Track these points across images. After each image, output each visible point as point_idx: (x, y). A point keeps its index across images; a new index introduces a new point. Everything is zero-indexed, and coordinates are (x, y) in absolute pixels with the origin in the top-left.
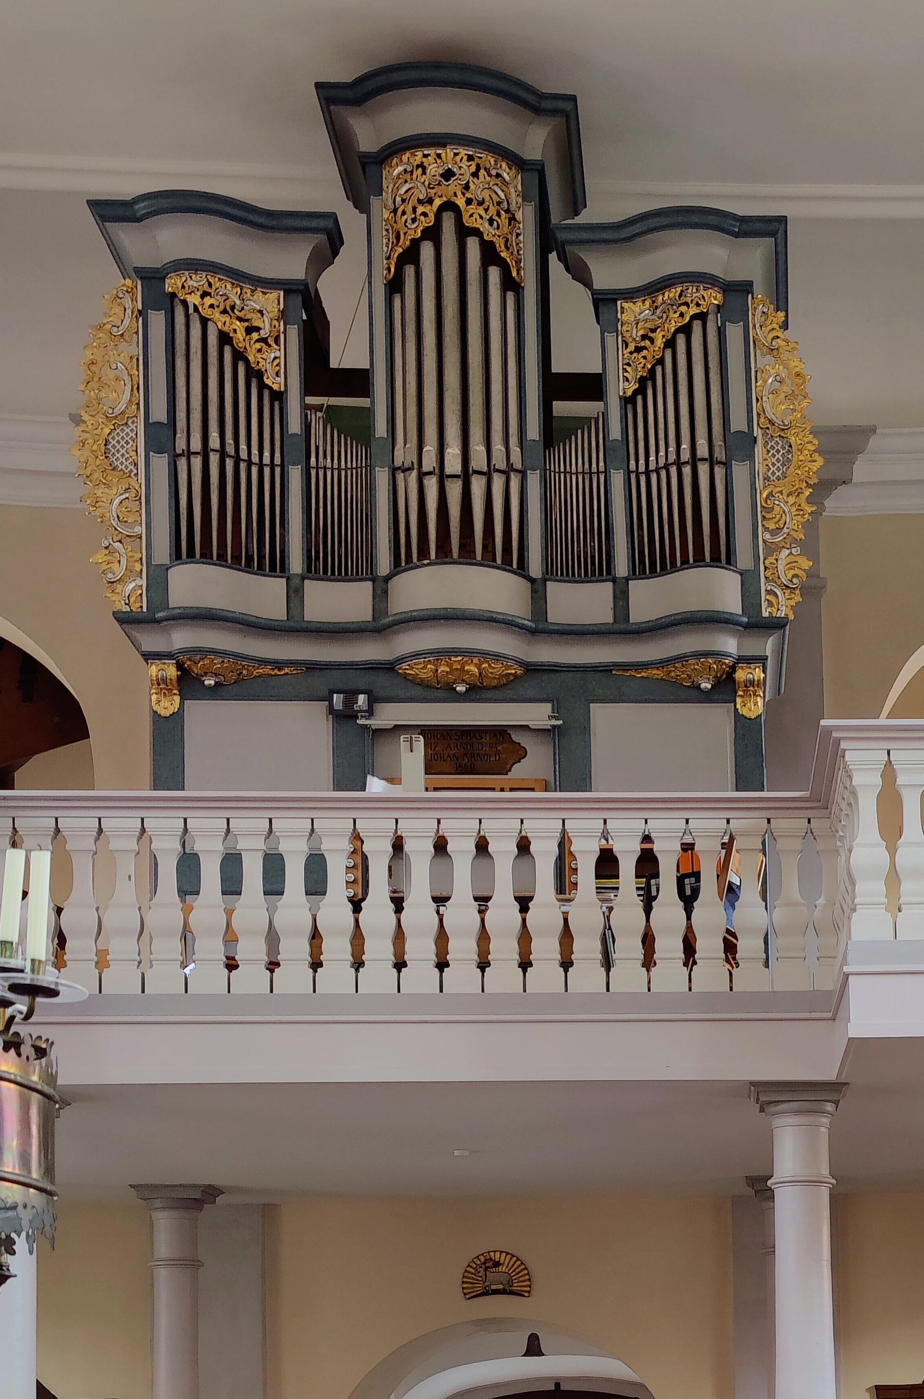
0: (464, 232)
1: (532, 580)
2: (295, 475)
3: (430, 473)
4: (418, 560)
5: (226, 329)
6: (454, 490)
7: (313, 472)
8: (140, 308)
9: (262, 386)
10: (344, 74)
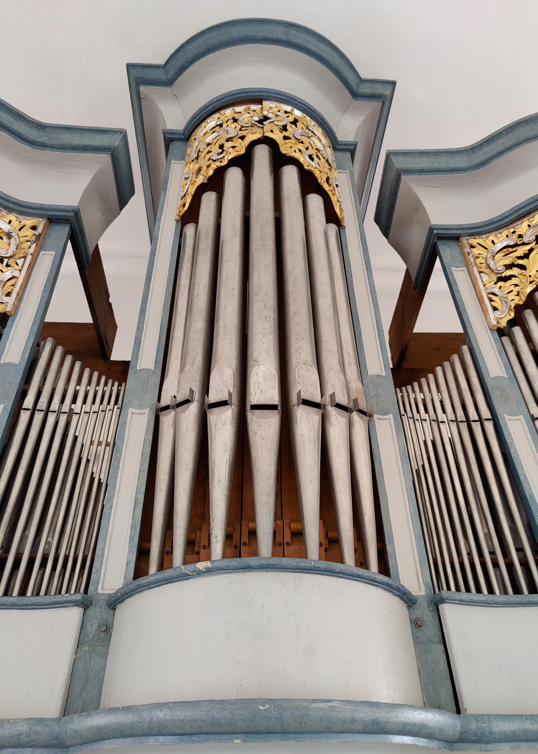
0: (279, 160)
1: (409, 600)
3: (223, 403)
4: (185, 562)
6: (264, 432)
7: (24, 417)
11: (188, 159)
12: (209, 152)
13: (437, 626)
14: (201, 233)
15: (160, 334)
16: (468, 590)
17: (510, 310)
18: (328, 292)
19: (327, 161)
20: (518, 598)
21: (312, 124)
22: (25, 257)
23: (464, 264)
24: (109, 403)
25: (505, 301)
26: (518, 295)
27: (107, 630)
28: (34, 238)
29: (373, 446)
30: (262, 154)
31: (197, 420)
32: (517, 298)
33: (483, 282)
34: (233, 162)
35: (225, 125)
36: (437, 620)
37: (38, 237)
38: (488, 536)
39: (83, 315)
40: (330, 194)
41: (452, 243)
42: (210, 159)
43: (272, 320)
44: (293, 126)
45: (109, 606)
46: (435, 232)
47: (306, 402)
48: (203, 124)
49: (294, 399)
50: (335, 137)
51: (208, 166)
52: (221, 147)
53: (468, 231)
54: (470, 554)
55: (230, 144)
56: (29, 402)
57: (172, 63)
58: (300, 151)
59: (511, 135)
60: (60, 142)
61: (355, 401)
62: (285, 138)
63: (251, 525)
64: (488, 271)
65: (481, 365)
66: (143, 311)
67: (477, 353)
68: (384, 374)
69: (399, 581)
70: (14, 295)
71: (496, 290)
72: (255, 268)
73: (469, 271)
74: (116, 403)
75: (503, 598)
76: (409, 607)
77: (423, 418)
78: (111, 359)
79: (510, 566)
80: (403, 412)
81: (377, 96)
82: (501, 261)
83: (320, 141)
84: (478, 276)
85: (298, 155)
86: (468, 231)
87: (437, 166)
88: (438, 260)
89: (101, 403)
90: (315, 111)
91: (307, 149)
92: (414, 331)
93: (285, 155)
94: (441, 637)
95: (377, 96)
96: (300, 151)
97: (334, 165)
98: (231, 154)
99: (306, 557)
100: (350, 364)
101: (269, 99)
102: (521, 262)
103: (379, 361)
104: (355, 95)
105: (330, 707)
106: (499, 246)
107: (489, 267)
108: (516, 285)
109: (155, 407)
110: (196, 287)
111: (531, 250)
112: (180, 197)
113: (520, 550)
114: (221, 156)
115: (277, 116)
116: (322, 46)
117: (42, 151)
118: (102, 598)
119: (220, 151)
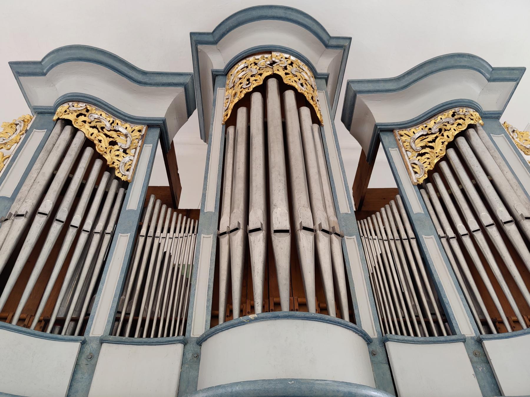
0: (283, 87)
1: (368, 340)
2: (123, 243)
5: (92, 138)
7: (141, 240)
8: (28, 129)
9: (113, 176)
10: (207, 26)
11: (227, 87)
12: (241, 83)
13: (385, 355)
14: (239, 131)
15: (217, 191)
16: (402, 334)
17: (425, 173)
18: (315, 165)
19: (311, 86)
20: (432, 338)
21: (301, 64)
22: (136, 148)
23: (396, 146)
24: (189, 232)
25: (421, 167)
26: (429, 164)
27: (197, 357)
28: (140, 137)
29: (345, 258)
30: (273, 84)
31: (242, 240)
32: (429, 166)
33: (408, 157)
34: (256, 89)
35: (249, 67)
36: (384, 352)
37: (143, 136)
38: (414, 306)
39: (164, 182)
40: (314, 106)
41: (389, 134)
42: (241, 88)
43: (283, 182)
44: (291, 66)
45: (198, 344)
46: (378, 127)
47: (305, 228)
48: (236, 66)
49: (298, 226)
50: (316, 71)
51: (241, 92)
52: (248, 80)
53: (399, 126)
54: (404, 317)
55: (253, 78)
56: (143, 231)
57: (217, 31)
58: (295, 81)
59: (421, 70)
60: (155, 82)
61: (333, 228)
62: (286, 74)
63: (276, 300)
64: (411, 150)
65: (408, 206)
66: (206, 178)
67: (405, 199)
68: (350, 213)
69: (361, 327)
70: (131, 170)
71: (416, 162)
72: (272, 152)
73: (399, 150)
74: (193, 232)
75: (423, 339)
76: (368, 344)
77: (374, 238)
78: (179, 208)
79: (428, 323)
80: (362, 235)
81: (341, 46)
82: (419, 144)
83: (307, 74)
84: (405, 153)
85: (294, 84)
86: (399, 126)
87: (377, 88)
88: (381, 143)
89: (185, 232)
90: (303, 57)
91: (299, 80)
92: (368, 187)
93: (286, 84)
94: (387, 361)
95: (341, 46)
96: (295, 81)
97: (316, 88)
98: (255, 85)
99: (308, 311)
100: (329, 207)
101: (275, 51)
102: (430, 144)
103: (347, 205)
104: (327, 46)
105: (326, 383)
106: (417, 135)
107: (411, 148)
108: (428, 158)
109: (216, 234)
110: (238, 164)
111: (436, 137)
112: (224, 110)
113: (433, 314)
114: (249, 86)
115: (281, 61)
116: (307, 19)
117: (144, 87)
118: (193, 339)
119: (248, 82)
